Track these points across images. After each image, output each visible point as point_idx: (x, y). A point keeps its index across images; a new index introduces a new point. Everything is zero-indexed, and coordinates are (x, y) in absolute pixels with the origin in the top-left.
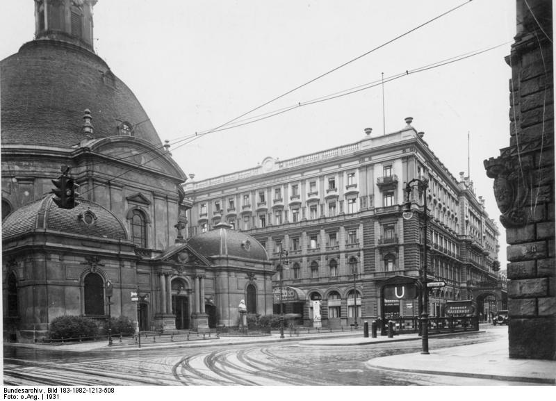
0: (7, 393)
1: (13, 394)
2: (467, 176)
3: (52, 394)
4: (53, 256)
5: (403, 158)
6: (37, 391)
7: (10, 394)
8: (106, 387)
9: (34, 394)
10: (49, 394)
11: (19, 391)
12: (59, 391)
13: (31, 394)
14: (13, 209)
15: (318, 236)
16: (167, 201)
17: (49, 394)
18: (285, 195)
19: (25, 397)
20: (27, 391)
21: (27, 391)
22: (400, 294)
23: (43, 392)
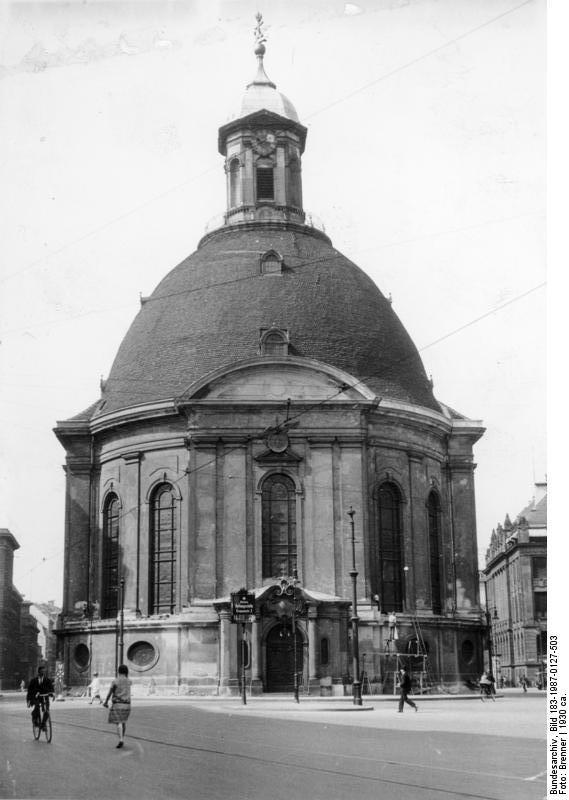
0: (557, 790)
1: (559, 781)
7: (559, 786)
11: (554, 772)
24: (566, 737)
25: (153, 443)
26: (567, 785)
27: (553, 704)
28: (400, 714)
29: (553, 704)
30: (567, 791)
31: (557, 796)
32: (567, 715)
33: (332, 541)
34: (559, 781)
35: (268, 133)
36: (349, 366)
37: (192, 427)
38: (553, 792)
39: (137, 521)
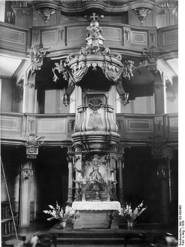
0: (181, 244)
1: (182, 241)
2: (162, 72)
3: (182, 224)
4: (129, 61)
5: (92, 39)
6: (181, 230)
7: (182, 243)
8: (179, 214)
9: (182, 232)
10: (182, 225)
11: (180, 238)
12: (180, 221)
13: (182, 233)
14: (110, 2)
15: (90, 108)
16: (165, 60)
17: (182, 225)
18: (137, 58)
19: (183, 236)
20: (181, 235)
21: (181, 235)
22: (114, 214)
23: (181, 228)
24: (184, 229)
25: (13, 57)
26: (184, 242)
27: (180, 217)
28: (66, 46)
29: (180, 217)
30: (184, 244)
31: (182, 246)
32: (184, 222)
33: (74, 78)
34: (182, 241)
35: (27, 155)
36: (120, 122)
37: (158, 8)
38: (180, 245)
39: (63, 49)
